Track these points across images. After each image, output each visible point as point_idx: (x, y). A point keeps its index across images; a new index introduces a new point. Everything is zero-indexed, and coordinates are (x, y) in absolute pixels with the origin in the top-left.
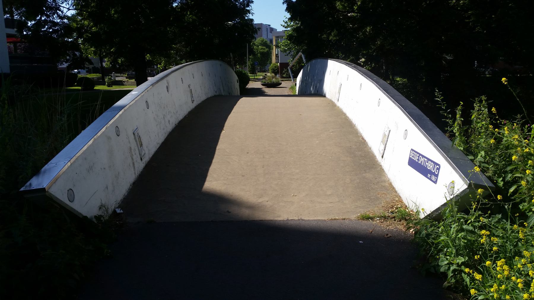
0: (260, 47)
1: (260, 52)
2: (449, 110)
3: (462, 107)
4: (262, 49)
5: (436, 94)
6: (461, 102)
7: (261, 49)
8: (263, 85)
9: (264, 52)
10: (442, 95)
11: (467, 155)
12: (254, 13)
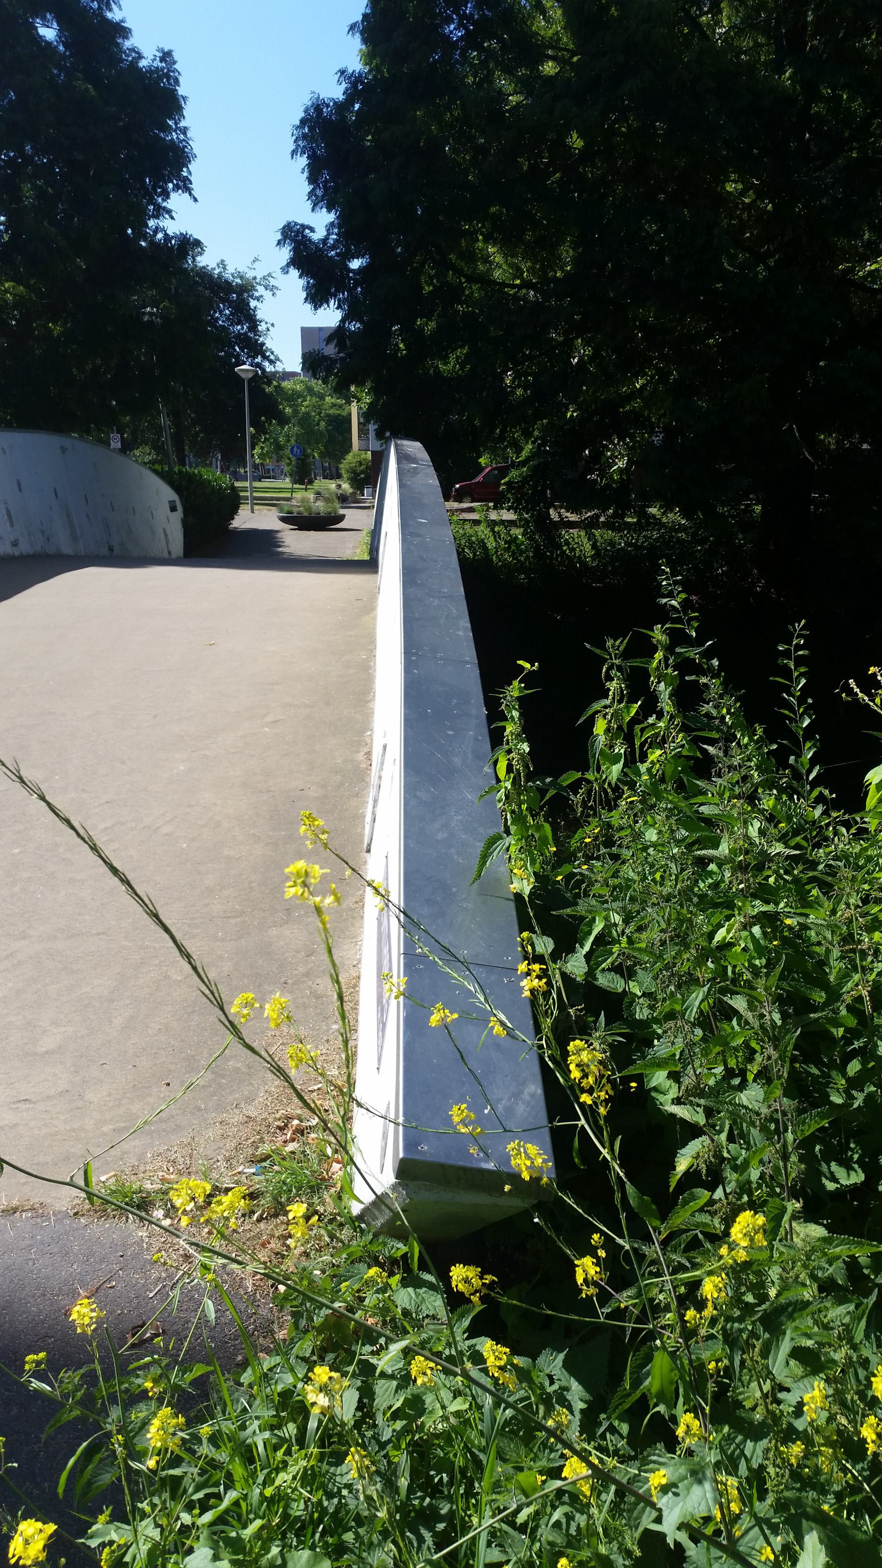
0: (328, 399)
1: (328, 415)
2: (710, 643)
3: (525, 688)
4: (334, 405)
5: (664, 583)
6: (520, 662)
7: (332, 408)
8: (283, 520)
9: (340, 415)
10: (687, 587)
11: (524, 925)
12: (277, 288)
